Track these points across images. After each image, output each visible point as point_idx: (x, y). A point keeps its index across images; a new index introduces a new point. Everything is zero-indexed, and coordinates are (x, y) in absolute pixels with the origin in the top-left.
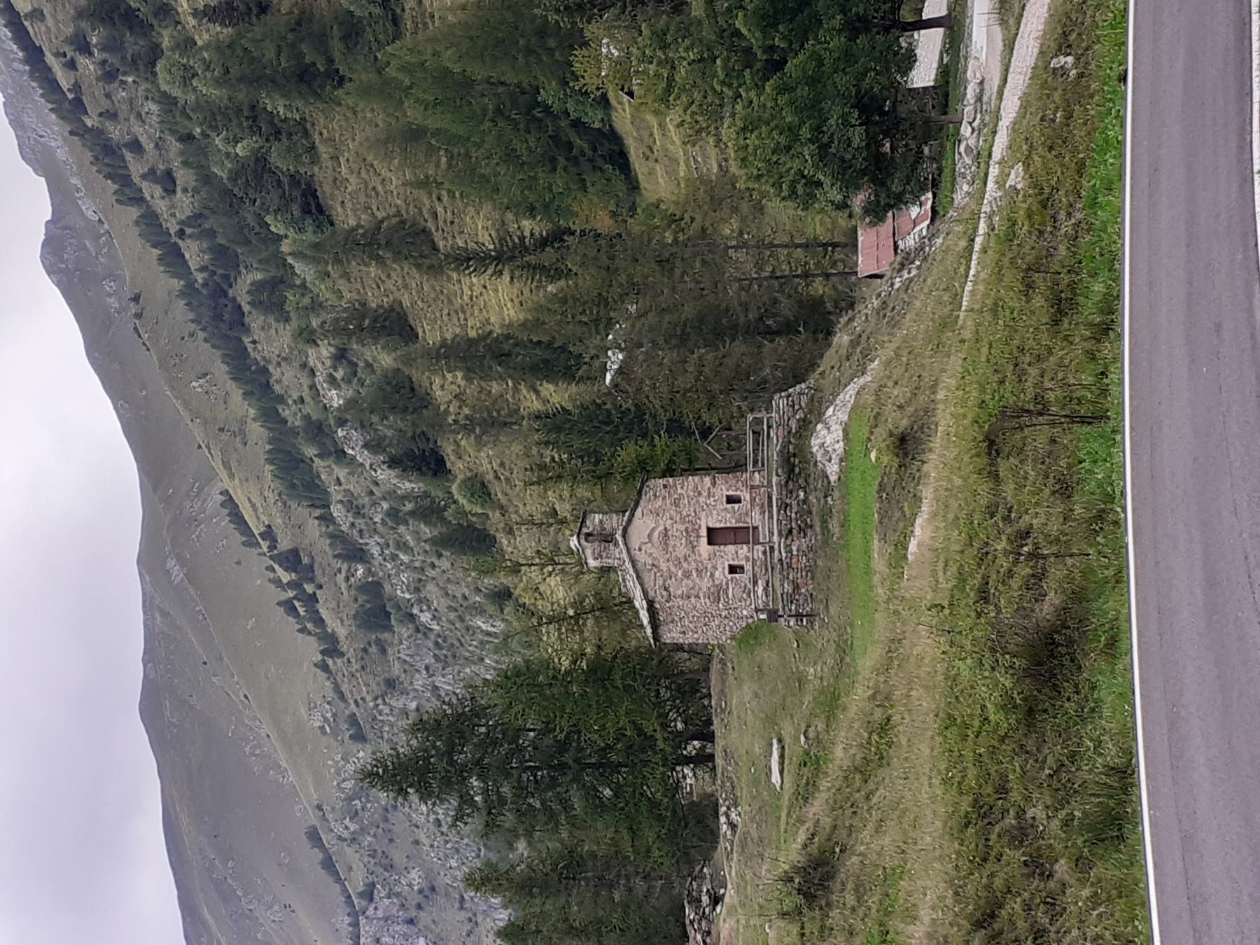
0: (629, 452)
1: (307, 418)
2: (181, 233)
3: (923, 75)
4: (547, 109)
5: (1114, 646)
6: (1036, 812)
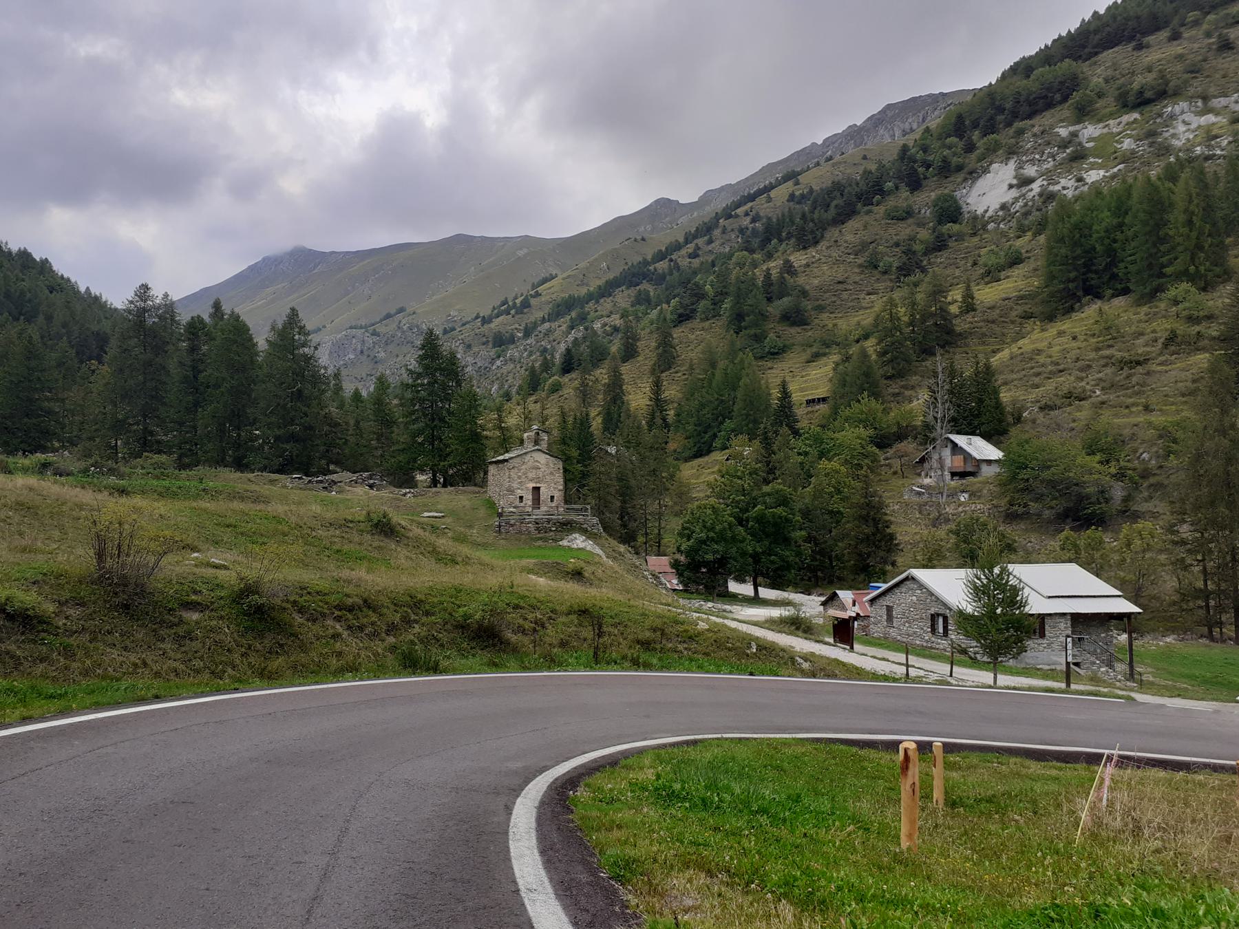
0: (575, 453)
1: (588, 313)
2: (671, 260)
3: (733, 587)
4: (722, 423)
5: (494, 666)
6: (417, 628)
